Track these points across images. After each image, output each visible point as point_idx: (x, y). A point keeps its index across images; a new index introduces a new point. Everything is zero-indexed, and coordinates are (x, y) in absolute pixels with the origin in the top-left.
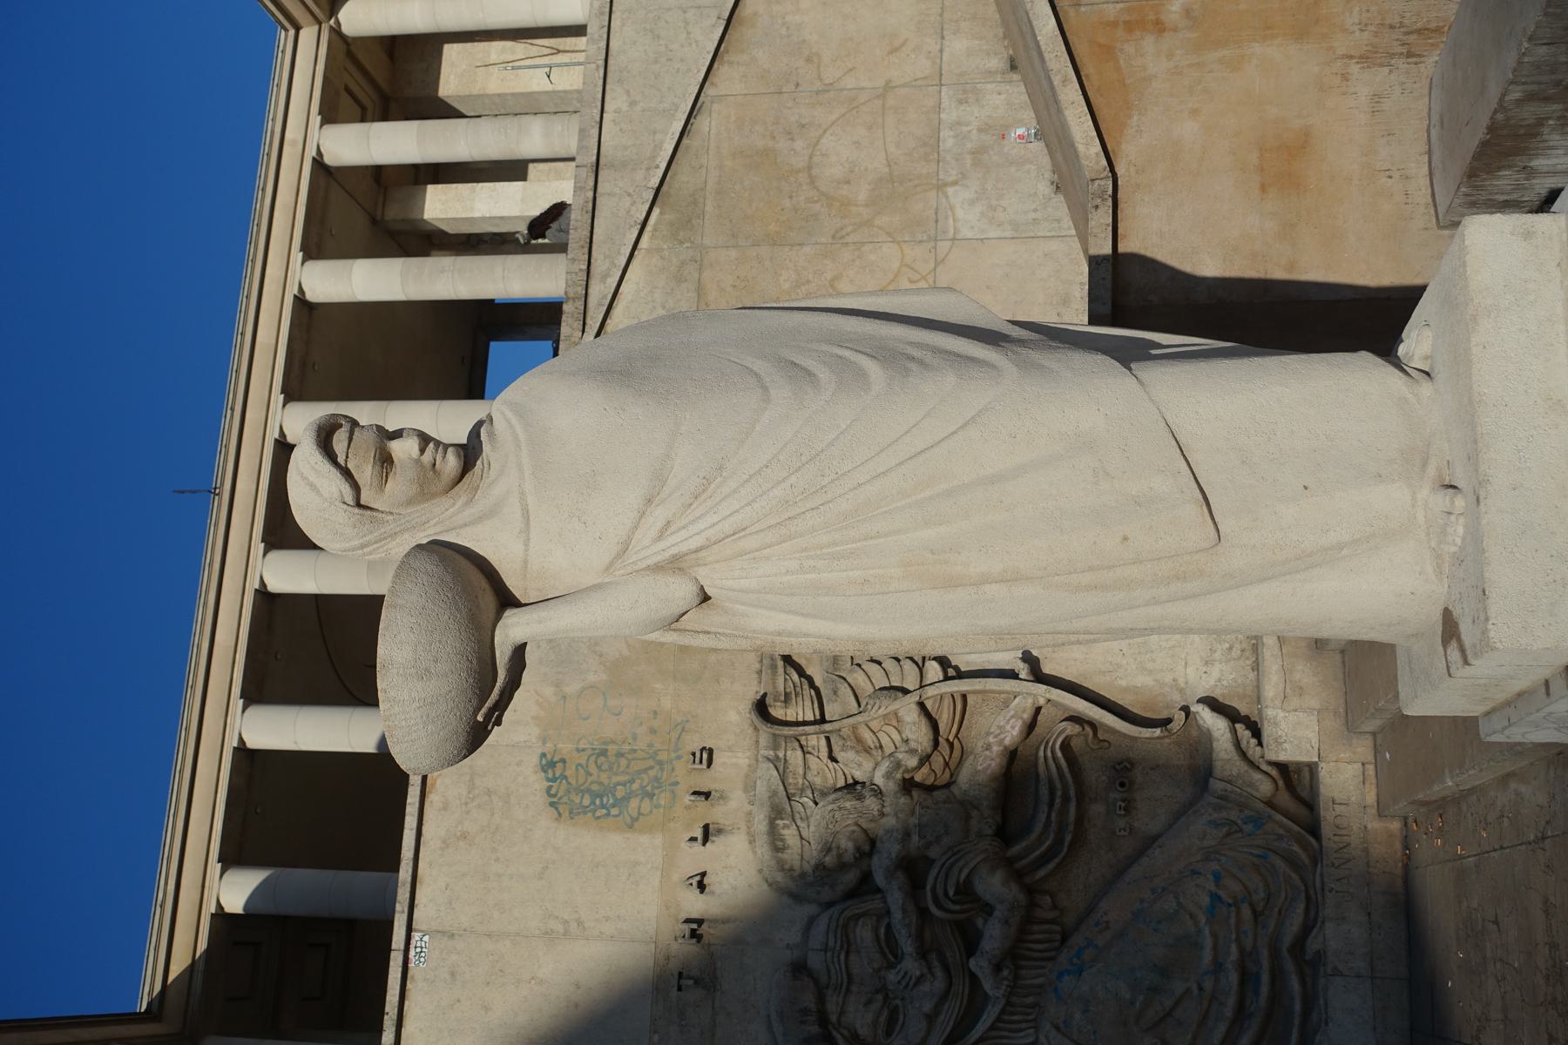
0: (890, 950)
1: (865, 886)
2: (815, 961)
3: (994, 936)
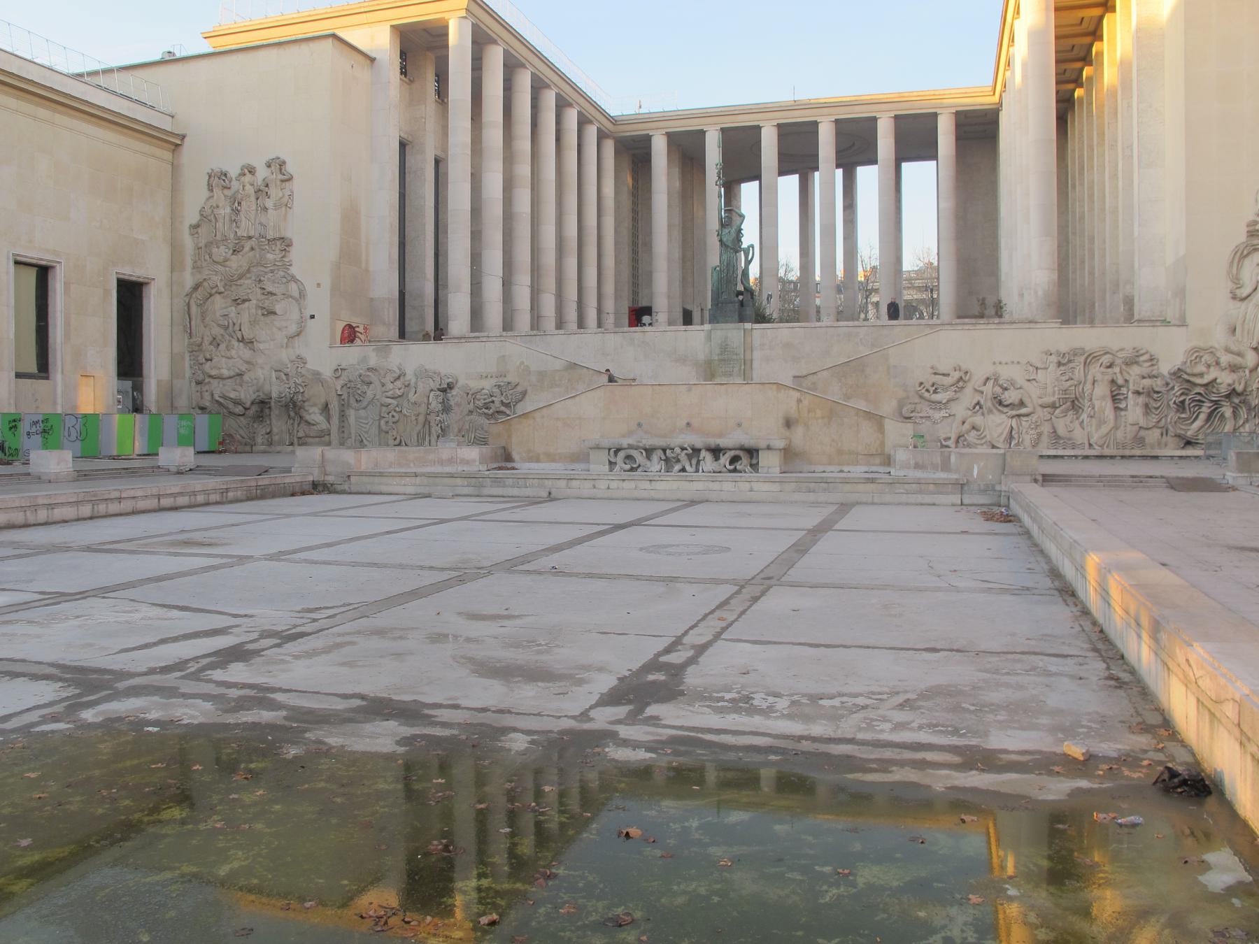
0: (484, 400)
1: (491, 396)
2: (483, 391)
3: (486, 411)
